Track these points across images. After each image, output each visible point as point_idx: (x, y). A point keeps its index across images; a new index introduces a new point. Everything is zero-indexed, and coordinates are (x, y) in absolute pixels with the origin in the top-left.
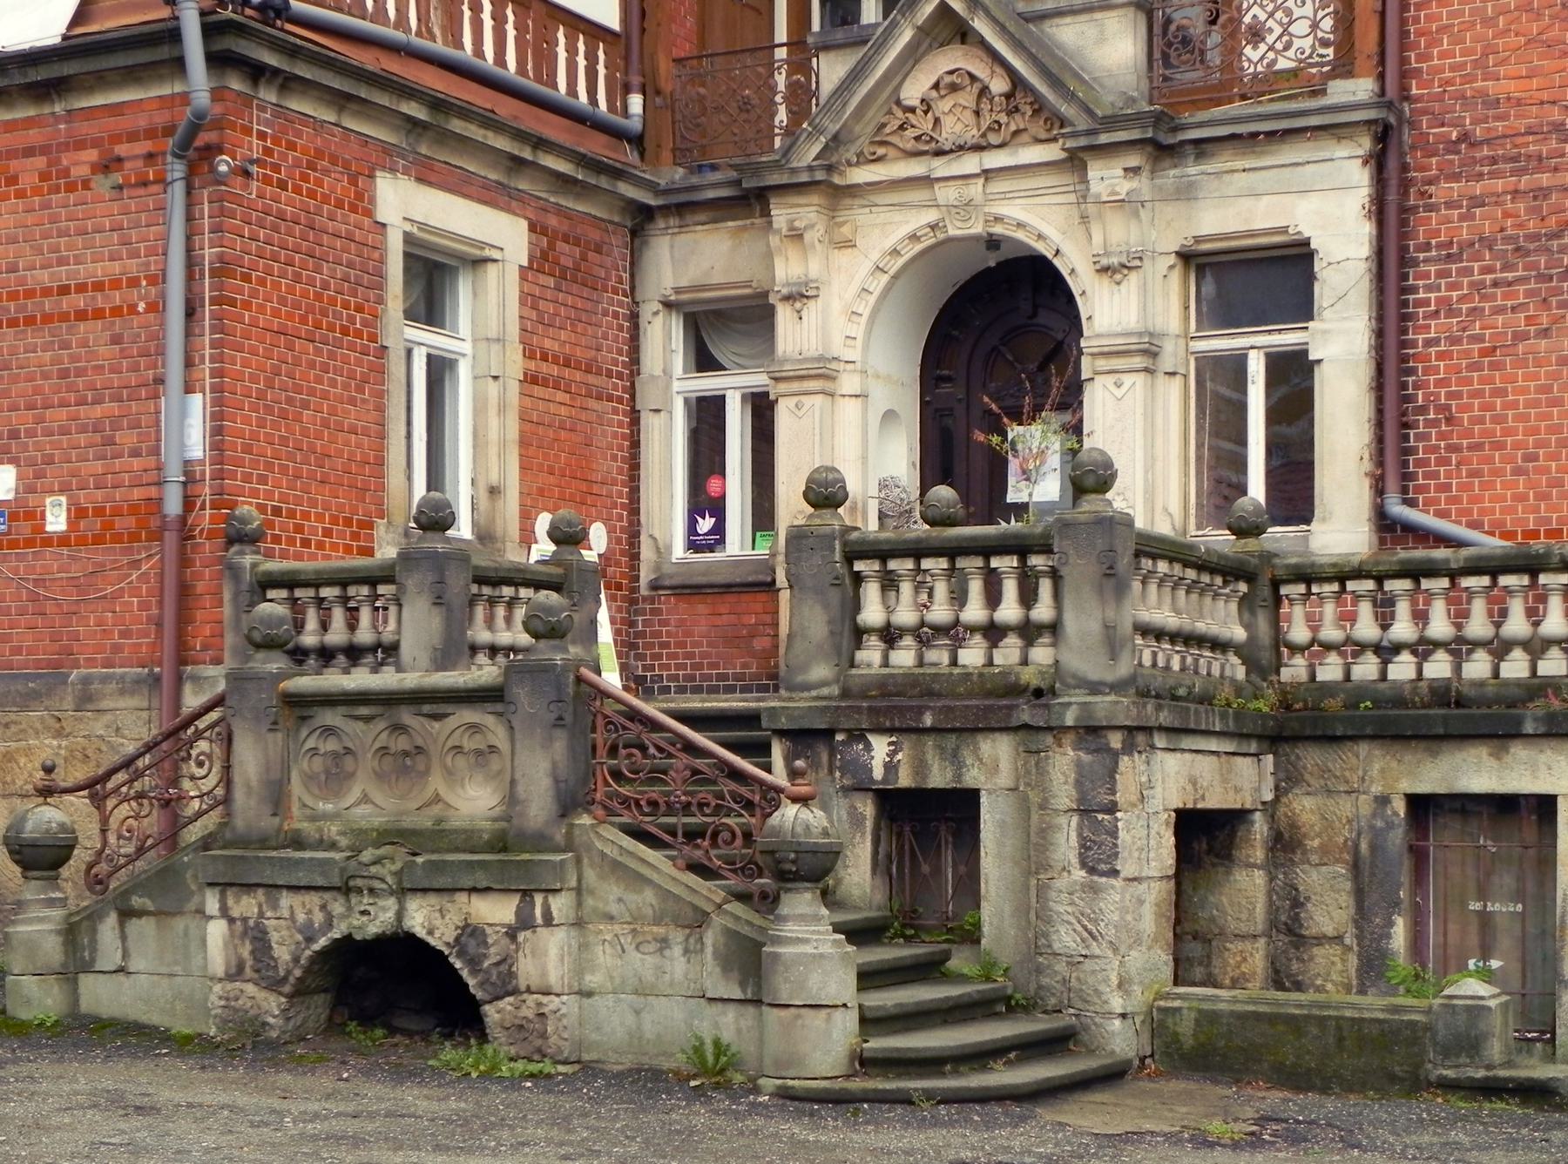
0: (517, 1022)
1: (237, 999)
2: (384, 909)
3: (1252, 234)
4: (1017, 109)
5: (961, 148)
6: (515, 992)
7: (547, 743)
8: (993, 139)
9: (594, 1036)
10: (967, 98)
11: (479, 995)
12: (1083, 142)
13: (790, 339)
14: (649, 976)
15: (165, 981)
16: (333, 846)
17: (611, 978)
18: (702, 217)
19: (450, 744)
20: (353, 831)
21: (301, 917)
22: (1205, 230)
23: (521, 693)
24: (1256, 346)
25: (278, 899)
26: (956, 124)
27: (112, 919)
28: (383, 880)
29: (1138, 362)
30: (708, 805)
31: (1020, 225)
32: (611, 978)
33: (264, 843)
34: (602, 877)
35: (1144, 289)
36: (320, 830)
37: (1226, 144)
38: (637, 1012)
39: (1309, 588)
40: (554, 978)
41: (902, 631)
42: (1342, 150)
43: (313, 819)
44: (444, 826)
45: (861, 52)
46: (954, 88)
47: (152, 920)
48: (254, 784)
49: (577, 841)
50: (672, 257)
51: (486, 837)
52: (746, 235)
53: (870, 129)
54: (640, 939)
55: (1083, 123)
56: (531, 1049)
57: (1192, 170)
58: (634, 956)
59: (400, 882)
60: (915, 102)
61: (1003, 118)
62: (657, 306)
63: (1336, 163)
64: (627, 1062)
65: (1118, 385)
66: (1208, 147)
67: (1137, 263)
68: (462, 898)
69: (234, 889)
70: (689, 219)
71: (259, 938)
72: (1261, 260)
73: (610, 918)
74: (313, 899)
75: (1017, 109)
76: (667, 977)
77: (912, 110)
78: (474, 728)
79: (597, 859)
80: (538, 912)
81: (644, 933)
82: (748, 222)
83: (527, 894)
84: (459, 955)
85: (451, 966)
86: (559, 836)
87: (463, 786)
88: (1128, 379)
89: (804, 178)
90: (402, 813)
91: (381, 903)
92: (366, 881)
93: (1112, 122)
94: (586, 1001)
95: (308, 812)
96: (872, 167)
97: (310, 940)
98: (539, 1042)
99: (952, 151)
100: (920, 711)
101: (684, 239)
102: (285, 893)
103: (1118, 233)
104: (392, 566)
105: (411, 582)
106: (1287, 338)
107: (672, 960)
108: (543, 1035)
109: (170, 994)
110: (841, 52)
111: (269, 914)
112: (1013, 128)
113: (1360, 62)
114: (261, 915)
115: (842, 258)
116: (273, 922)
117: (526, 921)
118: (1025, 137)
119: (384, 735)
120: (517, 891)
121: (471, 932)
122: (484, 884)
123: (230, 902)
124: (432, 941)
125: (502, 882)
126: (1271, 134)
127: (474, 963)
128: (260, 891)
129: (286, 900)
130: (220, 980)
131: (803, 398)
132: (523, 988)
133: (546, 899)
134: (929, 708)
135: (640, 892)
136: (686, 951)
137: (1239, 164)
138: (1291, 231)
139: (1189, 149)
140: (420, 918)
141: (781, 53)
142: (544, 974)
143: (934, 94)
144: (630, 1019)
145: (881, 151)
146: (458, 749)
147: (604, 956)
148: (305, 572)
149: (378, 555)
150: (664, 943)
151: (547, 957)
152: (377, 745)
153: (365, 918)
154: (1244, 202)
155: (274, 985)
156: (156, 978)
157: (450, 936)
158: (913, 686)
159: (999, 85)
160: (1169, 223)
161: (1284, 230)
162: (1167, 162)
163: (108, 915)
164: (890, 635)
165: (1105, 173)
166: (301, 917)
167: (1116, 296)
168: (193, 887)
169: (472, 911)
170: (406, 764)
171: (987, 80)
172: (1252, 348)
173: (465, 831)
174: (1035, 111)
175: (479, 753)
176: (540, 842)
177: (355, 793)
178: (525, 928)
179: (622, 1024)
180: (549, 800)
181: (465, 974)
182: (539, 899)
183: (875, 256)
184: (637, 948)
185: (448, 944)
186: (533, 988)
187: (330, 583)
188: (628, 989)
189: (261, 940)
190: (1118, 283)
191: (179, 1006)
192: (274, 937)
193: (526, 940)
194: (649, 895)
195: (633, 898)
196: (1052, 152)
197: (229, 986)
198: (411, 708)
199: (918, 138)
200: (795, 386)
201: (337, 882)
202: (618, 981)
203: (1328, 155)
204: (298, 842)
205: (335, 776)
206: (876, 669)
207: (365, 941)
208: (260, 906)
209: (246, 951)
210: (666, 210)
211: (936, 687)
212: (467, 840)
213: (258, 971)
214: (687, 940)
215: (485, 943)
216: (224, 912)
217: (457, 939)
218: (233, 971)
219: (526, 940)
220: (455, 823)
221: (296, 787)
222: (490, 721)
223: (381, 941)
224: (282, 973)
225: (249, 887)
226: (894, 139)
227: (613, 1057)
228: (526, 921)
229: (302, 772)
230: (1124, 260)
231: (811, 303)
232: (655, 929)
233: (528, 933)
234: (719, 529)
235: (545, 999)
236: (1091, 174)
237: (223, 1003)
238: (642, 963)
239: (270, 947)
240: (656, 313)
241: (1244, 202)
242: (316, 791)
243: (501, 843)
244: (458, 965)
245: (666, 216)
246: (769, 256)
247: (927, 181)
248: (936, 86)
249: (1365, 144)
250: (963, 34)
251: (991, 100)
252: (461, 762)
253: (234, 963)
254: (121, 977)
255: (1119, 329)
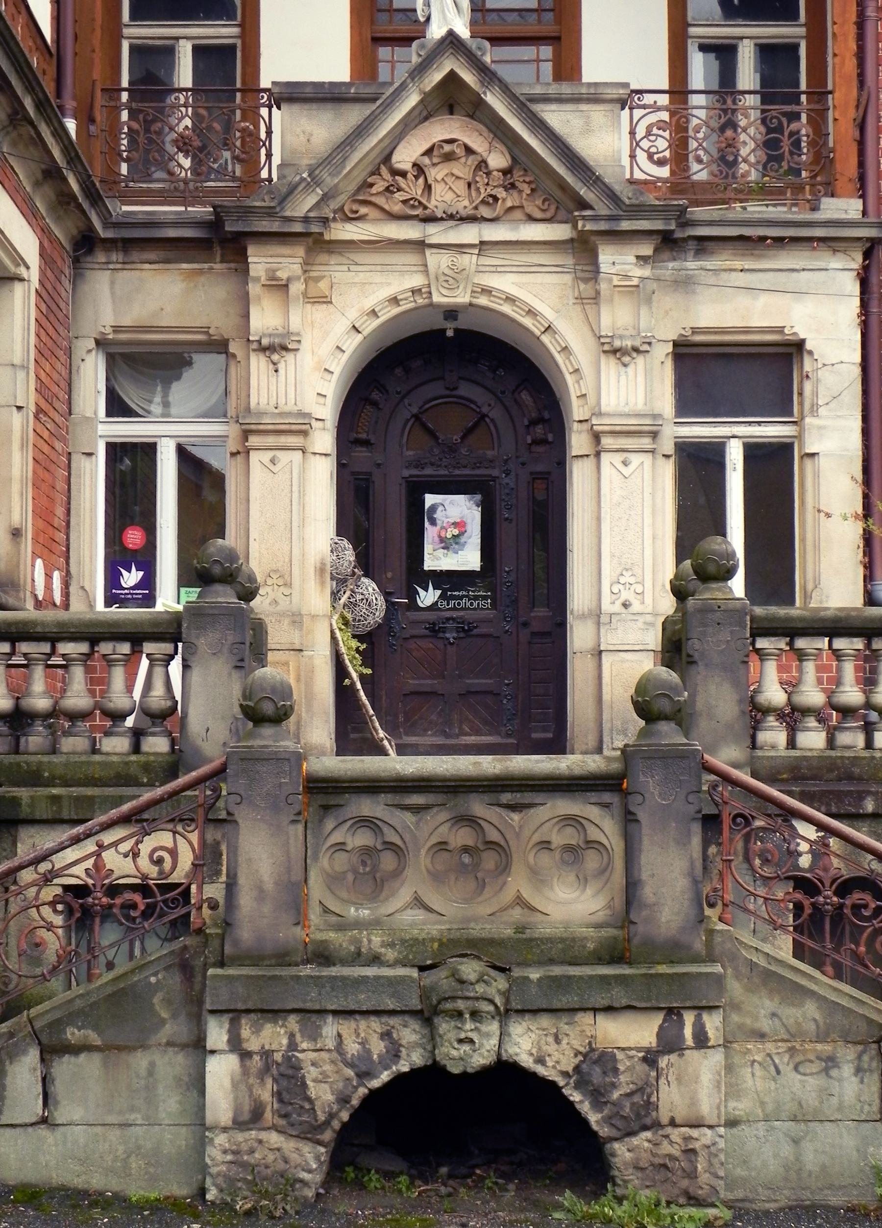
0: (657, 1161)
1: (252, 1151)
2: (488, 1035)
3: (747, 330)
4: (513, 186)
5: (451, 217)
6: (656, 1125)
7: (683, 842)
8: (485, 212)
9: (740, 1172)
10: (462, 169)
11: (604, 1131)
12: (603, 226)
13: (264, 393)
14: (811, 1100)
15: (114, 1135)
16: (376, 960)
17: (762, 1104)
18: (152, 256)
19: (536, 838)
20: (403, 941)
21: (352, 1048)
22: (704, 322)
23: (651, 785)
24: (735, 437)
25: (319, 1027)
26: (447, 191)
27: (33, 1056)
28: (491, 1001)
29: (646, 442)
30: (866, 906)
31: (510, 299)
32: (762, 1104)
33: (283, 958)
34: (750, 989)
35: (647, 373)
36: (357, 941)
37: (729, 245)
38: (796, 1142)
39: (53, 648)
40: (707, 1108)
41: (806, 711)
42: (836, 262)
43: (341, 928)
44: (528, 934)
45: (367, 110)
46: (449, 157)
47: (96, 1059)
48: (269, 885)
49: (718, 950)
50: (113, 294)
51: (591, 946)
52: (202, 279)
53: (352, 187)
54: (799, 1058)
55: (602, 208)
56: (676, 1191)
57: (691, 265)
58: (790, 1077)
59: (507, 1001)
60: (407, 166)
61: (501, 193)
62: (92, 344)
63: (831, 273)
64: (784, 1198)
65: (625, 463)
66: (710, 245)
67: (645, 347)
68: (586, 1019)
69: (252, 1016)
70: (135, 255)
71: (289, 1077)
72: (739, 355)
73: (761, 1036)
74: (376, 1024)
75: (513, 186)
76: (835, 1101)
77: (403, 174)
78: (571, 820)
79: (744, 970)
80: (688, 1032)
81: (805, 1052)
82: (206, 266)
83: (673, 1013)
84: (577, 1086)
85: (565, 1099)
86: (699, 945)
87: (552, 889)
88: (636, 459)
89: (298, 228)
90: (468, 920)
91: (484, 1028)
92: (469, 1003)
93: (637, 211)
94: (734, 1131)
95: (334, 919)
96: (349, 227)
97: (363, 1075)
98: (685, 1183)
99: (442, 219)
100: (860, 797)
101: (127, 277)
102: (330, 1019)
103: (617, 317)
104: (176, 619)
105: (203, 643)
106: (772, 431)
107: (840, 1080)
108: (692, 1175)
109: (121, 1148)
110: (307, 106)
111: (304, 1045)
112: (509, 204)
113: (841, 184)
114: (293, 1045)
115: (319, 312)
116: (312, 1055)
117: (669, 1043)
118: (518, 214)
119: (444, 829)
120: (660, 1009)
121: (597, 1062)
122: (624, 1002)
123: (245, 1032)
124: (541, 1070)
125: (649, 999)
126: (779, 240)
127: (598, 1097)
128: (293, 1019)
129: (330, 1028)
130: (225, 1130)
131: (279, 454)
132: (665, 1120)
133: (698, 1018)
134: (869, 793)
135: (801, 1005)
136: (858, 1070)
137: (738, 264)
138: (786, 331)
139: (692, 245)
140: (526, 1044)
141: (125, 96)
142: (694, 1102)
143: (426, 160)
144: (787, 1150)
145: (363, 210)
146: (545, 845)
147: (753, 1080)
148: (43, 624)
149: (159, 607)
150: (830, 1062)
151: (696, 1084)
152: (434, 840)
153: (466, 1047)
154: (737, 302)
155: (309, 1132)
156: (99, 1129)
157: (568, 1063)
158: (830, 770)
159: (497, 160)
160: (667, 313)
161: (780, 330)
162: (666, 255)
163: (25, 1052)
164: (793, 716)
165: (617, 258)
166: (352, 1048)
167: (623, 379)
168: (164, 1015)
169: (600, 1035)
170: (481, 860)
171: (485, 154)
172: (734, 437)
173: (562, 940)
174: (532, 190)
175: (569, 849)
176: (675, 951)
177: (405, 895)
178: (670, 1051)
179: (776, 1156)
180: (686, 903)
181: (585, 1107)
182: (689, 1018)
183: (353, 314)
184: (796, 1068)
185: (566, 1074)
186: (678, 1121)
187: (74, 638)
188: (784, 1116)
189: (290, 1077)
190: (625, 365)
191: (135, 1164)
192: (311, 1073)
193: (670, 1065)
194: (811, 1009)
195: (792, 1014)
196: (560, 232)
197: (240, 1137)
198: (487, 798)
199: (404, 202)
200: (271, 440)
201: (415, 1003)
202: (770, 1108)
203: (822, 265)
204: (323, 956)
205: (372, 874)
206: (782, 750)
207: (465, 1074)
208: (292, 1036)
209: (266, 1093)
210: (110, 244)
211: (857, 771)
212: (567, 950)
213: (285, 1116)
214: (859, 1057)
215: (616, 1071)
216: (236, 1045)
217: (577, 1069)
218: (246, 1116)
219: (670, 1065)
220: (544, 930)
221: (316, 889)
222: (594, 812)
223: (485, 1072)
224: (322, 1117)
225: (274, 1014)
226: (380, 201)
227: (763, 1194)
228: (669, 1043)
229: (323, 871)
230: (637, 343)
231: (290, 357)
232: (819, 1047)
233: (673, 1057)
234: (149, 583)
235: (695, 1133)
236: (602, 258)
237: (229, 1157)
238: (803, 1086)
239: (304, 1085)
240: (89, 351)
241: (737, 302)
242: (344, 895)
243: (615, 953)
244: (576, 1097)
245: (107, 250)
246: (244, 304)
247: (421, 245)
248: (429, 152)
249: (856, 261)
250: (477, 110)
251: (488, 174)
252: (545, 859)
253: (246, 1108)
254: (43, 1131)
255: (626, 410)
